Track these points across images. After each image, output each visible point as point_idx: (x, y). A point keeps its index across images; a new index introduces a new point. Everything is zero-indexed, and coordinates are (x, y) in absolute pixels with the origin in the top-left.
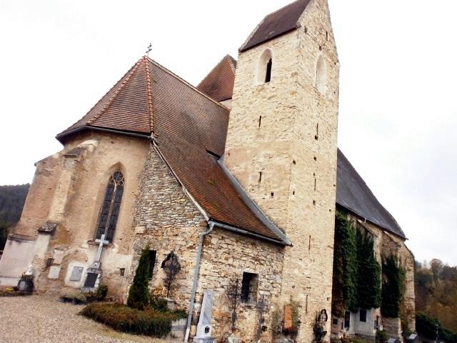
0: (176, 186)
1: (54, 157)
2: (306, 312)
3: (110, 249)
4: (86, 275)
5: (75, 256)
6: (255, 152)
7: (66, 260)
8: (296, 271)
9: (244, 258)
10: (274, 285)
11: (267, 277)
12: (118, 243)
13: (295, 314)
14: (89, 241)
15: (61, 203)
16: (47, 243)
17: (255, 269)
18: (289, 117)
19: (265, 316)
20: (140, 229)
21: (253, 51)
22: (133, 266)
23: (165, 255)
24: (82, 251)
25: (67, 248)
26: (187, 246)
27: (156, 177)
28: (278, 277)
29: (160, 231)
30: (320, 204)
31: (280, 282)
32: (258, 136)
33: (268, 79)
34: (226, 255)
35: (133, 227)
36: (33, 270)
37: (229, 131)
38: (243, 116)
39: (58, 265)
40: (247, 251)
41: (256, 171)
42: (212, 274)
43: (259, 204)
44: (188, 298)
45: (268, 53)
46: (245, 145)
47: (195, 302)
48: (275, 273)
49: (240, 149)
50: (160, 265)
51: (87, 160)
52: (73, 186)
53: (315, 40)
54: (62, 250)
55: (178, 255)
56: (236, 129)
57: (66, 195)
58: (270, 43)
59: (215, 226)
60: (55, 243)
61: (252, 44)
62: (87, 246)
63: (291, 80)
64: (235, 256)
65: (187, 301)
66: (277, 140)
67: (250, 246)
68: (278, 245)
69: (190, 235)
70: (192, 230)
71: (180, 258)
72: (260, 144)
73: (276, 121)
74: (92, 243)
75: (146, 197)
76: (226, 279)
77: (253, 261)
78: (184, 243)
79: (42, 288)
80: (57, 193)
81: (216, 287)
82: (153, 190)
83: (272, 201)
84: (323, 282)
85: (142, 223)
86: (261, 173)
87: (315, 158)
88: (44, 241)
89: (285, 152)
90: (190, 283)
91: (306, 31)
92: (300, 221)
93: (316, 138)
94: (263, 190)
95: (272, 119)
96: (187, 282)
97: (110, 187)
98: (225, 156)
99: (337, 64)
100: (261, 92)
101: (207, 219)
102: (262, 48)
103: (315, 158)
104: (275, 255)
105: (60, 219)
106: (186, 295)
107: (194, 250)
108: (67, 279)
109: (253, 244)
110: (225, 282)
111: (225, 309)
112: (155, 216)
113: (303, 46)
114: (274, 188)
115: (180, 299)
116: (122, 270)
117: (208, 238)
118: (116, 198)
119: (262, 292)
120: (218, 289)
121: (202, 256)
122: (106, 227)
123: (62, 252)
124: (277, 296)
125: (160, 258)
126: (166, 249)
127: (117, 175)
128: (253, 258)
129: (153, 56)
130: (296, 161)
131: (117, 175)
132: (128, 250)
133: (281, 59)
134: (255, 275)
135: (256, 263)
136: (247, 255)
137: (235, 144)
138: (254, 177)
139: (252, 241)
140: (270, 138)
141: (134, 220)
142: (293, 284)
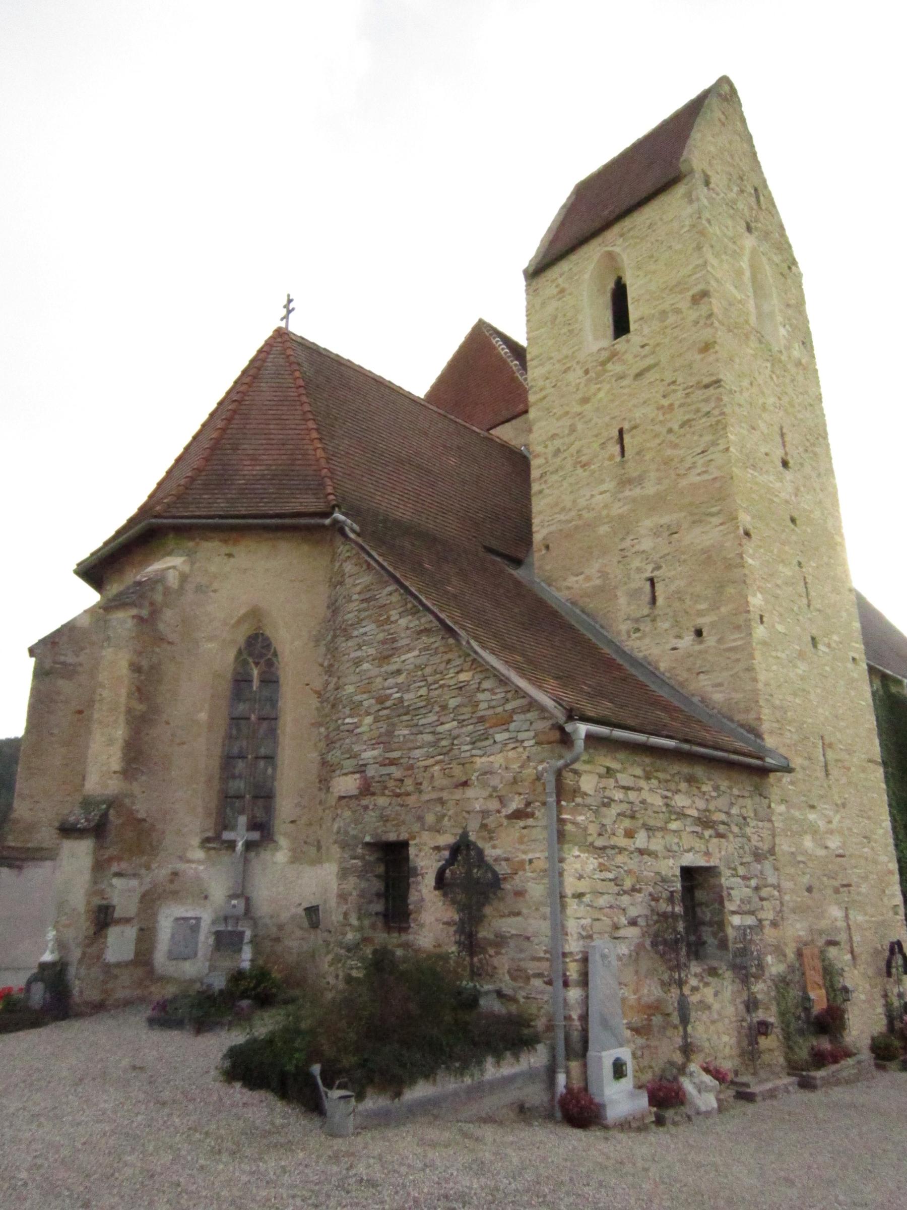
0: (435, 641)
1: (78, 624)
2: (854, 958)
3: (266, 855)
4: (211, 941)
5: (174, 888)
6: (624, 526)
7: (150, 901)
9: (673, 826)
10: (764, 892)
11: (741, 871)
12: (285, 834)
13: (829, 973)
14: (207, 840)
15: (111, 742)
17: (707, 854)
18: (708, 414)
19: (759, 988)
20: (347, 784)
21: (564, 266)
22: (343, 897)
23: (437, 848)
24: (189, 869)
25: (148, 868)
26: (505, 812)
27: (370, 627)
28: (767, 865)
29: (409, 782)
30: (829, 646)
31: (775, 882)
32: (625, 482)
33: (621, 326)
34: (627, 823)
35: (324, 782)
36: (61, 945)
37: (535, 487)
38: (566, 440)
39: (127, 921)
40: (680, 801)
41: (637, 577)
42: (600, 886)
43: (663, 666)
44: (539, 975)
45: (611, 257)
46: (586, 515)
47: (566, 984)
48: (758, 856)
49: (577, 528)
50: (430, 880)
52: (139, 689)
53: (732, 204)
54: (135, 875)
55: (480, 844)
56: (555, 477)
57: (122, 718)
58: (612, 234)
59: (589, 737)
60: (110, 860)
61: (560, 247)
62: (200, 854)
63: (693, 315)
64: (652, 823)
65: (537, 983)
66: (684, 483)
67: (683, 786)
68: (752, 768)
69: (509, 776)
70: (510, 758)
71: (490, 853)
72: (634, 500)
73: (670, 431)
74: (217, 842)
75: (350, 689)
76: (639, 897)
77: (699, 829)
78: (493, 805)
79: (95, 995)
80: (96, 716)
81: (616, 927)
82: (366, 666)
83: (700, 652)
84: (875, 862)
85: (349, 764)
86: (652, 581)
87: (793, 520)
88: (78, 856)
89: (714, 510)
90: (538, 925)
91: (707, 183)
92: (790, 698)
93: (785, 464)
94: (666, 625)
95: (657, 428)
96: (521, 923)
97: (241, 682)
98: (538, 555)
99: (793, 268)
100: (609, 366)
101: (560, 716)
102: (593, 252)
103: (793, 520)
104: (749, 802)
105: (114, 786)
106: (532, 967)
107: (530, 822)
108: (160, 956)
109: (691, 780)
110: (637, 906)
111: (652, 991)
112: (385, 740)
113: (709, 221)
114: (700, 614)
115: (514, 979)
116: (312, 912)
117: (569, 779)
119: (736, 920)
120: (622, 933)
121: (561, 836)
122: (245, 808)
123: (134, 883)
124: (774, 924)
125: (426, 862)
126: (437, 829)
127: (258, 648)
128: (699, 821)
129: (299, 327)
130: (752, 532)
131: (258, 648)
132: (319, 848)
133: (653, 267)
134: (709, 872)
135: (707, 833)
136: (681, 815)
137: (562, 517)
138: (634, 594)
139: (686, 769)
140: (659, 481)
141: (324, 763)
142: (806, 880)
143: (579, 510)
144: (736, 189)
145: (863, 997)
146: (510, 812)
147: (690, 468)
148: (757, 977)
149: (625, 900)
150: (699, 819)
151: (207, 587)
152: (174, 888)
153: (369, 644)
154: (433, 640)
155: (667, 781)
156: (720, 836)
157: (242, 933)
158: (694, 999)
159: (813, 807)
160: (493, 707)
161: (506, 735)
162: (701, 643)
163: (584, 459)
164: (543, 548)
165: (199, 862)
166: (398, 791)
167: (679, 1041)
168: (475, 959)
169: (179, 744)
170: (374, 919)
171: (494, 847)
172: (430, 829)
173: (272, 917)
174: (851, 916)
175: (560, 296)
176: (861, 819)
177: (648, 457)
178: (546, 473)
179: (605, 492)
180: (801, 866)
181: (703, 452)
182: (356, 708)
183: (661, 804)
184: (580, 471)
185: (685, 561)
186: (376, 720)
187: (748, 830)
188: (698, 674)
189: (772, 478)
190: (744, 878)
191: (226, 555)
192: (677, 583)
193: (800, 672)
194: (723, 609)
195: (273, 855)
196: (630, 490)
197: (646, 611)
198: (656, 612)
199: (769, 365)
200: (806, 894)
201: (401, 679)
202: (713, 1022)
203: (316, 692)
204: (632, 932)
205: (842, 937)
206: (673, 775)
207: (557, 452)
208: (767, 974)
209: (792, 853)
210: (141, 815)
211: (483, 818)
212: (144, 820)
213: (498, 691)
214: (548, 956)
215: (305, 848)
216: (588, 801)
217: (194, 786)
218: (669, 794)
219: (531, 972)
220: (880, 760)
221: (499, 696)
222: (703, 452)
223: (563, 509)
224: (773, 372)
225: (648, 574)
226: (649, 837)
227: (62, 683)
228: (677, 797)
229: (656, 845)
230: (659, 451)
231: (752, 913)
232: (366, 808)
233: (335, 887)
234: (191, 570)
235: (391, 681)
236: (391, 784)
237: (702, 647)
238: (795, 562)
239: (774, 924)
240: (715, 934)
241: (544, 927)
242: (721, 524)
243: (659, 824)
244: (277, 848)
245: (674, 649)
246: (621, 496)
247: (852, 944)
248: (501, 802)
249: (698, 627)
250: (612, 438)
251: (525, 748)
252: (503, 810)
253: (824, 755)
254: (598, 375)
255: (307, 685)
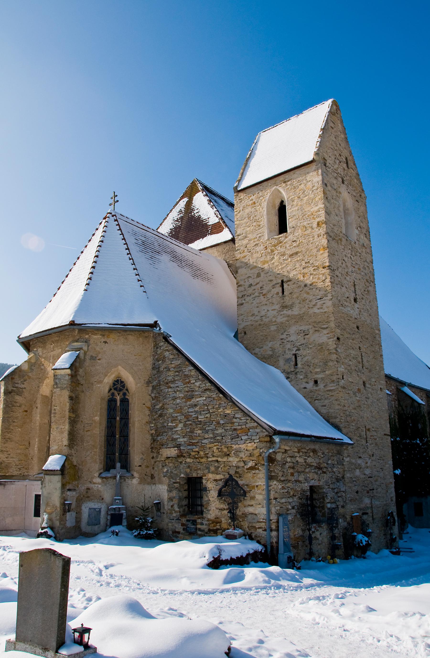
2: (373, 519)
5: (87, 495)
6: (283, 328)
8: (358, 472)
16: (59, 485)
22: (171, 499)
23: (216, 480)
24: (95, 487)
26: (246, 467)
27: (179, 383)
29: (202, 453)
34: (291, 471)
51: (81, 370)
57: (67, 421)
62: (99, 480)
71: (240, 482)
72: (288, 316)
76: (295, 499)
78: (242, 464)
82: (178, 401)
86: (295, 355)
97: (111, 402)
114: (316, 373)
118: (121, 413)
123: (74, 493)
124: (343, 507)
125: (212, 485)
127: (119, 385)
128: (316, 468)
137: (252, 318)
142: (355, 488)
143: (261, 317)
144: (337, 162)
145: (376, 535)
146: (248, 467)
147: (314, 305)
148: (336, 527)
149: (291, 500)
150: (316, 466)
151: (96, 357)
152: (87, 495)
153: (180, 391)
154: (212, 394)
155: (306, 452)
156: (324, 473)
157: (122, 514)
158: (313, 536)
159: (360, 457)
160: (241, 425)
161: (246, 437)
162: (317, 386)
163: (264, 292)
164: (243, 333)
165: (99, 484)
166: (197, 456)
167: (308, 551)
168: (235, 523)
169: (87, 431)
170: (184, 507)
171: (241, 480)
172: (213, 473)
173: (132, 507)
174: (373, 502)
175: (253, 206)
176: (379, 461)
177: (295, 296)
178: (245, 295)
179: (274, 310)
180: (355, 482)
181: (320, 299)
182: (174, 419)
183: (303, 462)
184: (262, 297)
185: (310, 348)
186: (185, 425)
187: (335, 470)
188: (315, 400)
189: (349, 309)
190: (332, 489)
191: (104, 342)
192: (307, 358)
193: (358, 398)
194: (327, 372)
195: (131, 481)
196: (287, 311)
197: (293, 369)
198: (297, 370)
199: (350, 251)
200: (356, 494)
201: (197, 409)
202: (319, 544)
203: (148, 407)
204: (294, 511)
205: (369, 511)
206: (308, 450)
207: (251, 285)
208: (339, 526)
209: (351, 478)
210: (75, 463)
211: (237, 469)
212: (76, 466)
213: (242, 419)
214: (264, 521)
215: (146, 477)
216: (279, 463)
217: (95, 450)
218: (306, 458)
219: (257, 527)
220: (389, 434)
221: (243, 421)
222: (320, 299)
223: (253, 315)
224: (351, 255)
225: (294, 352)
226: (299, 475)
227: (18, 398)
228: (309, 459)
229: (301, 478)
230: (300, 294)
231: (335, 502)
232: (181, 463)
233: (167, 495)
234: (88, 349)
235: (191, 410)
236: (193, 454)
237: (317, 388)
238: (358, 348)
239: (343, 507)
240: (320, 511)
241: (264, 511)
242: (327, 334)
243: (303, 470)
244: (133, 477)
245: (305, 388)
246: (282, 313)
247: (373, 514)
248: (244, 463)
249: (316, 379)
250: (278, 284)
251: (255, 443)
252: (245, 466)
253: (366, 435)
254: (272, 251)
255: (144, 404)
